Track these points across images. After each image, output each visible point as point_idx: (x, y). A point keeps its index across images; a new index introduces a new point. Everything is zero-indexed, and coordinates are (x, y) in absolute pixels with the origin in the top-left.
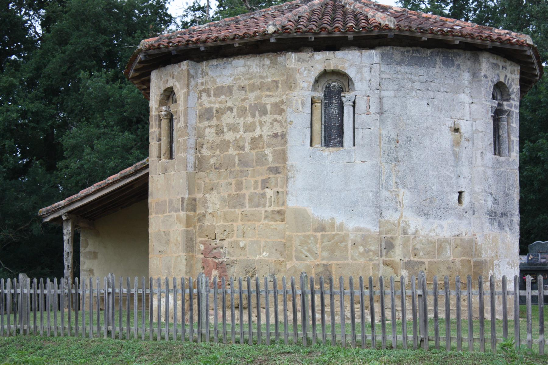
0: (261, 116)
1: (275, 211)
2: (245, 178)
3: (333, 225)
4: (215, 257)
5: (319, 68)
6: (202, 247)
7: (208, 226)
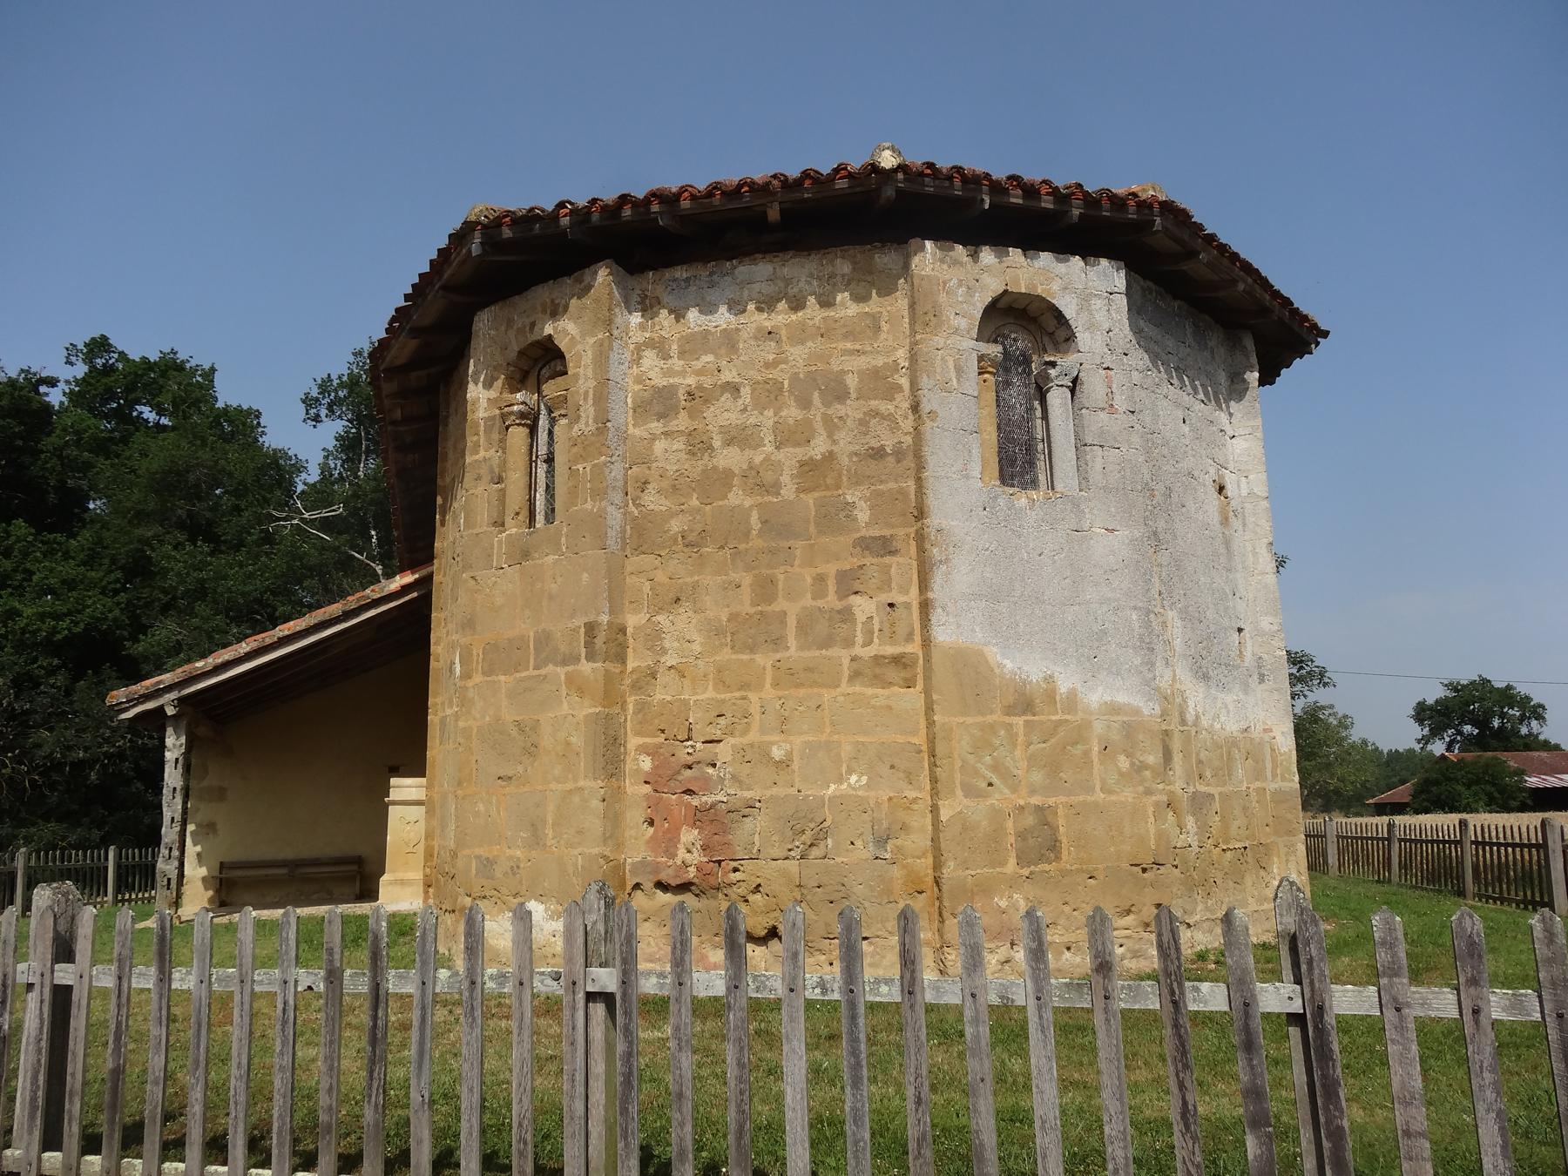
0: (827, 404)
1: (884, 657)
2: (782, 569)
3: (1051, 695)
4: (689, 792)
5: (992, 287)
6: (646, 764)
7: (663, 703)
